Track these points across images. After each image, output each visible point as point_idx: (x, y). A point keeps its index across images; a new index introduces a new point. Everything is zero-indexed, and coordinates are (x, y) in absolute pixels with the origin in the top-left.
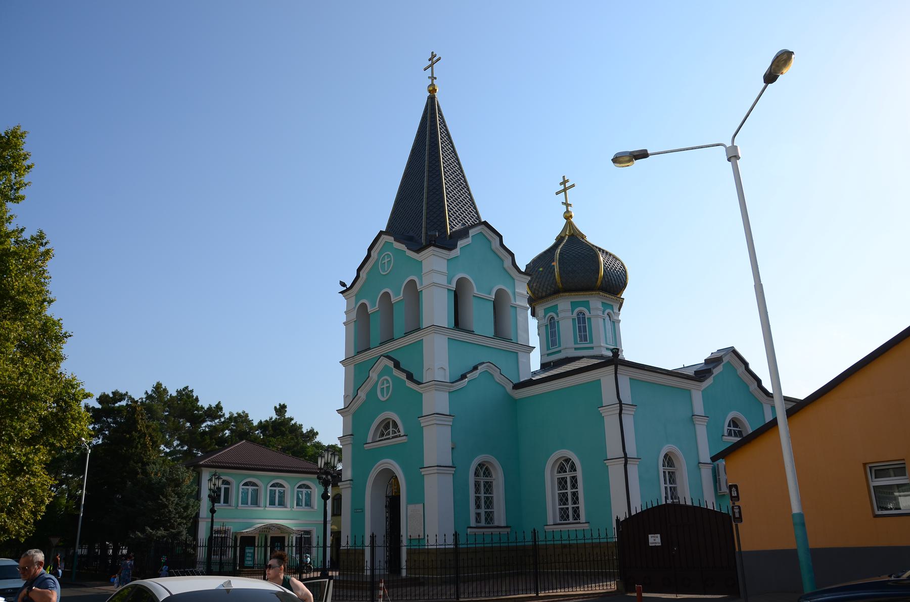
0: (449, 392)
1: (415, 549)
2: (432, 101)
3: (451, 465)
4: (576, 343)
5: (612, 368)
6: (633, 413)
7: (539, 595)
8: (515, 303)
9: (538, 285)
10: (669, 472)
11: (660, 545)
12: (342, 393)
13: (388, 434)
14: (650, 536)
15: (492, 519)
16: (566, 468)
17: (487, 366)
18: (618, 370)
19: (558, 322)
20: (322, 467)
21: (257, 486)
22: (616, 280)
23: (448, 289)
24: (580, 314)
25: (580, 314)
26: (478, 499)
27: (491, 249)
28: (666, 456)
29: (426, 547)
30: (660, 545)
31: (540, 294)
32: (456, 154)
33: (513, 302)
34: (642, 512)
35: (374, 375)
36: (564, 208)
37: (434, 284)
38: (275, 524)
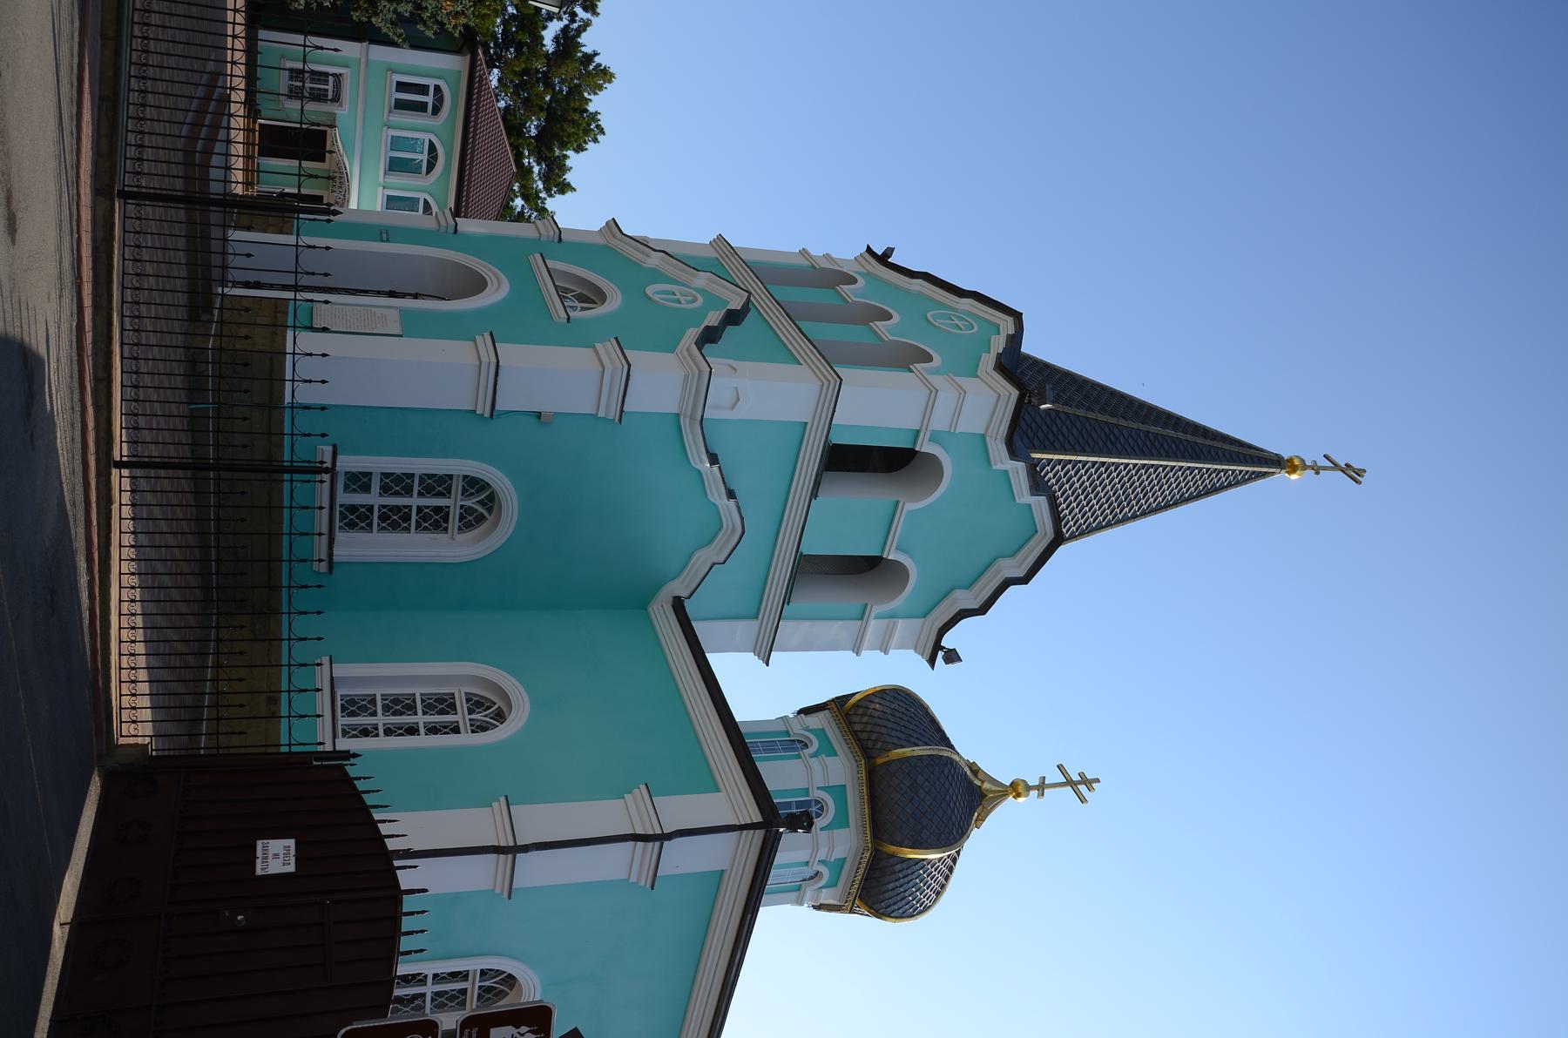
0: (678, 415)
1: (286, 313)
2: (1278, 462)
3: (497, 408)
5: (756, 817)
6: (633, 879)
7: (115, 472)
8: (873, 615)
9: (877, 714)
10: (464, 992)
11: (259, 872)
14: (291, 843)
15: (352, 526)
16: (478, 713)
17: (734, 529)
18: (752, 831)
19: (799, 757)
21: (427, 173)
22: (894, 893)
23: (918, 432)
27: (997, 558)
29: (284, 749)
30: (259, 872)
31: (856, 719)
32: (1176, 504)
33: (877, 609)
36: (1033, 781)
37: (933, 393)
38: (349, 198)
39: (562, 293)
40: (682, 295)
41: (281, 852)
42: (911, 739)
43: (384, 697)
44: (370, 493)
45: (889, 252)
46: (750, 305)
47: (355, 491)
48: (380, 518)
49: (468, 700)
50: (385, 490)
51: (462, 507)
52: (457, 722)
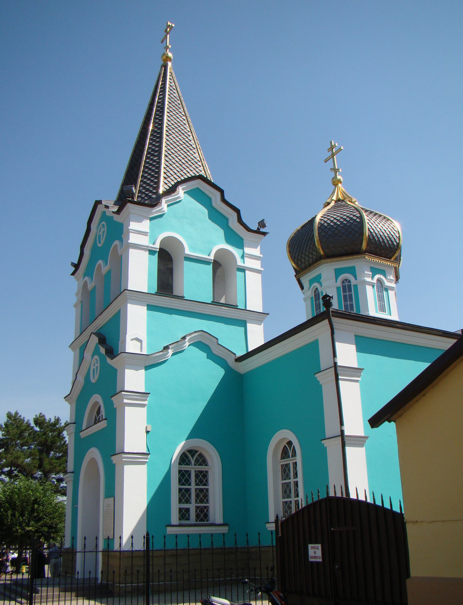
8: (242, 265)
11: (320, 560)
14: (310, 546)
15: (206, 516)
17: (201, 335)
24: (345, 281)
25: (345, 281)
30: (320, 560)
34: (308, 507)
39: (97, 421)
40: (94, 365)
41: (313, 550)
42: (310, 238)
43: (284, 498)
44: (190, 508)
45: (73, 264)
46: (98, 332)
47: (189, 515)
49: (284, 458)
50: (188, 501)
51: (195, 465)
52: (293, 463)
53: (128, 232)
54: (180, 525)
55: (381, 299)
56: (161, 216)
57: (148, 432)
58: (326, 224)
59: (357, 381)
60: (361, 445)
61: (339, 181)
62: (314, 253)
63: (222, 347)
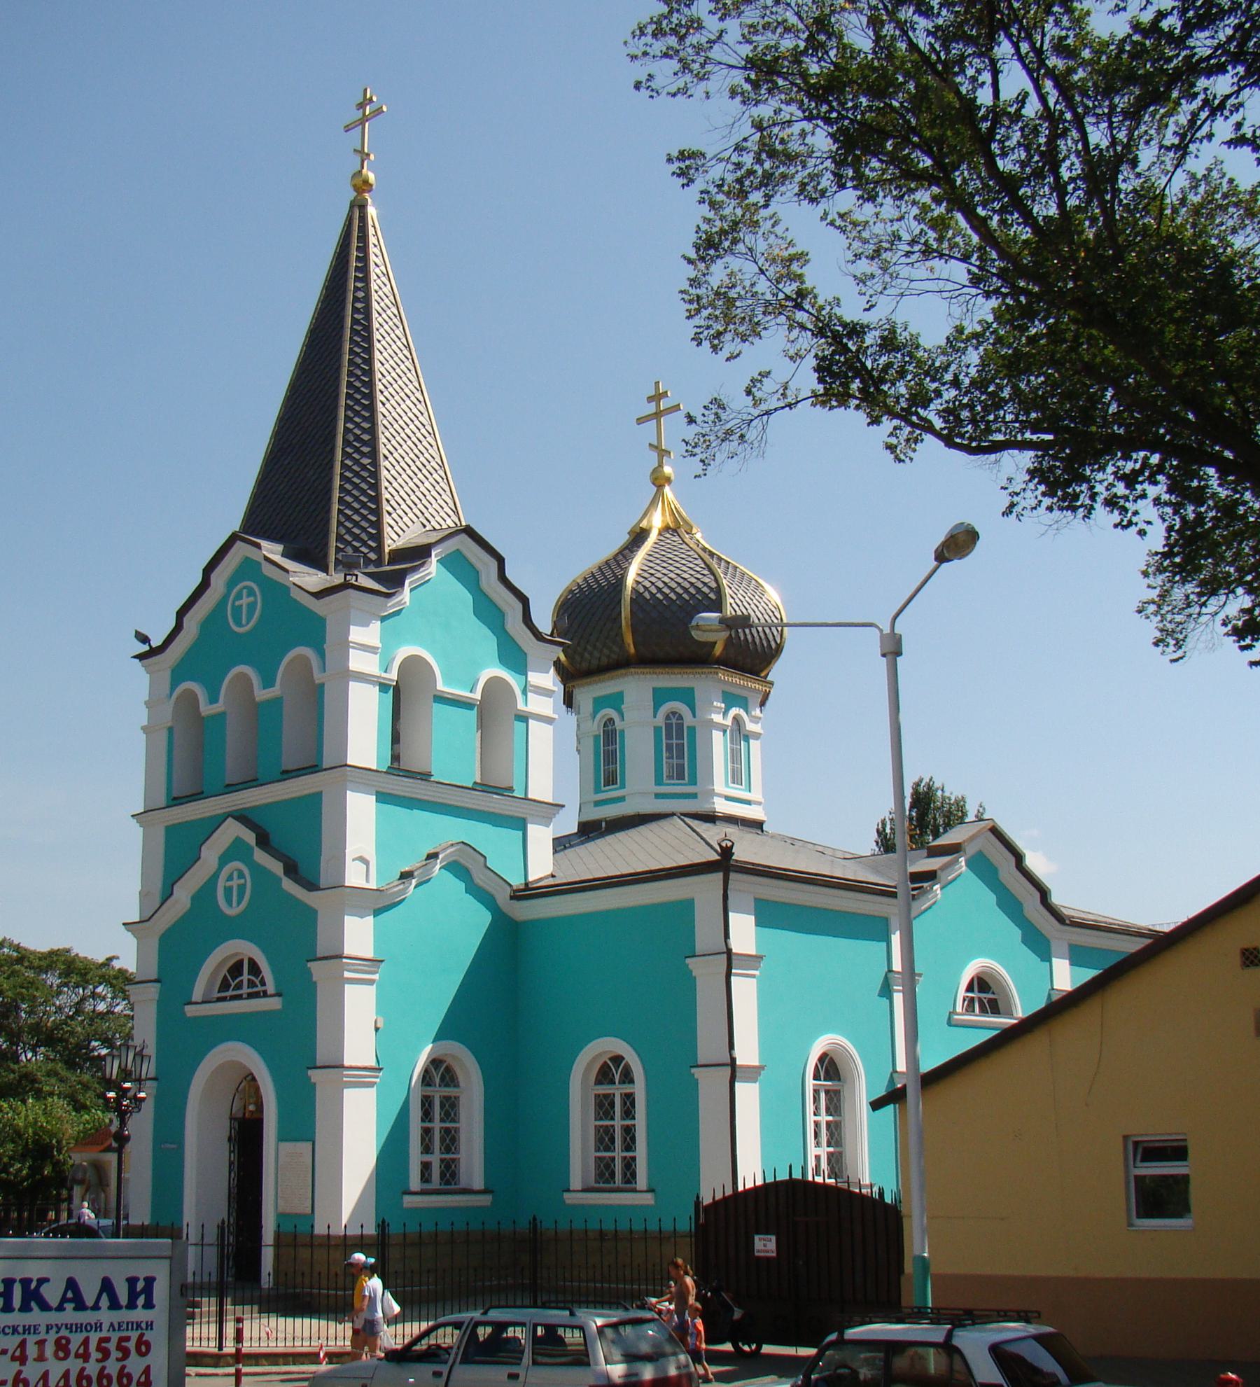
4: (659, 782)
5: (720, 875)
11: (774, 1254)
12: (136, 886)
13: (239, 986)
14: (757, 1237)
15: (454, 1175)
20: (114, 1077)
26: (427, 1132)
28: (822, 1058)
30: (774, 1254)
35: (211, 854)
41: (763, 1242)
43: (598, 1150)
48: (448, 1153)
53: (345, 645)
54: (423, 1192)
55: (735, 756)
56: (398, 613)
57: (377, 1029)
58: (647, 595)
59: (753, 976)
60: (754, 1080)
61: (668, 480)
62: (615, 649)
63: (492, 874)
